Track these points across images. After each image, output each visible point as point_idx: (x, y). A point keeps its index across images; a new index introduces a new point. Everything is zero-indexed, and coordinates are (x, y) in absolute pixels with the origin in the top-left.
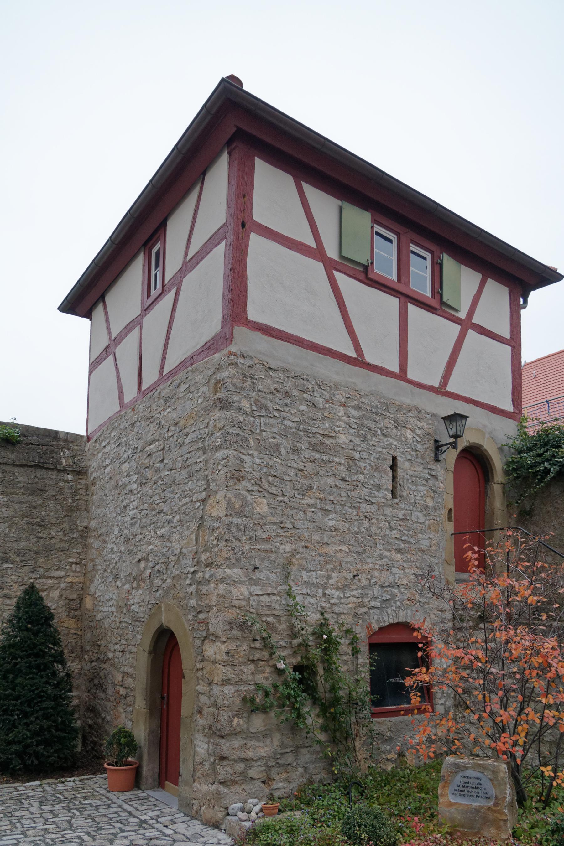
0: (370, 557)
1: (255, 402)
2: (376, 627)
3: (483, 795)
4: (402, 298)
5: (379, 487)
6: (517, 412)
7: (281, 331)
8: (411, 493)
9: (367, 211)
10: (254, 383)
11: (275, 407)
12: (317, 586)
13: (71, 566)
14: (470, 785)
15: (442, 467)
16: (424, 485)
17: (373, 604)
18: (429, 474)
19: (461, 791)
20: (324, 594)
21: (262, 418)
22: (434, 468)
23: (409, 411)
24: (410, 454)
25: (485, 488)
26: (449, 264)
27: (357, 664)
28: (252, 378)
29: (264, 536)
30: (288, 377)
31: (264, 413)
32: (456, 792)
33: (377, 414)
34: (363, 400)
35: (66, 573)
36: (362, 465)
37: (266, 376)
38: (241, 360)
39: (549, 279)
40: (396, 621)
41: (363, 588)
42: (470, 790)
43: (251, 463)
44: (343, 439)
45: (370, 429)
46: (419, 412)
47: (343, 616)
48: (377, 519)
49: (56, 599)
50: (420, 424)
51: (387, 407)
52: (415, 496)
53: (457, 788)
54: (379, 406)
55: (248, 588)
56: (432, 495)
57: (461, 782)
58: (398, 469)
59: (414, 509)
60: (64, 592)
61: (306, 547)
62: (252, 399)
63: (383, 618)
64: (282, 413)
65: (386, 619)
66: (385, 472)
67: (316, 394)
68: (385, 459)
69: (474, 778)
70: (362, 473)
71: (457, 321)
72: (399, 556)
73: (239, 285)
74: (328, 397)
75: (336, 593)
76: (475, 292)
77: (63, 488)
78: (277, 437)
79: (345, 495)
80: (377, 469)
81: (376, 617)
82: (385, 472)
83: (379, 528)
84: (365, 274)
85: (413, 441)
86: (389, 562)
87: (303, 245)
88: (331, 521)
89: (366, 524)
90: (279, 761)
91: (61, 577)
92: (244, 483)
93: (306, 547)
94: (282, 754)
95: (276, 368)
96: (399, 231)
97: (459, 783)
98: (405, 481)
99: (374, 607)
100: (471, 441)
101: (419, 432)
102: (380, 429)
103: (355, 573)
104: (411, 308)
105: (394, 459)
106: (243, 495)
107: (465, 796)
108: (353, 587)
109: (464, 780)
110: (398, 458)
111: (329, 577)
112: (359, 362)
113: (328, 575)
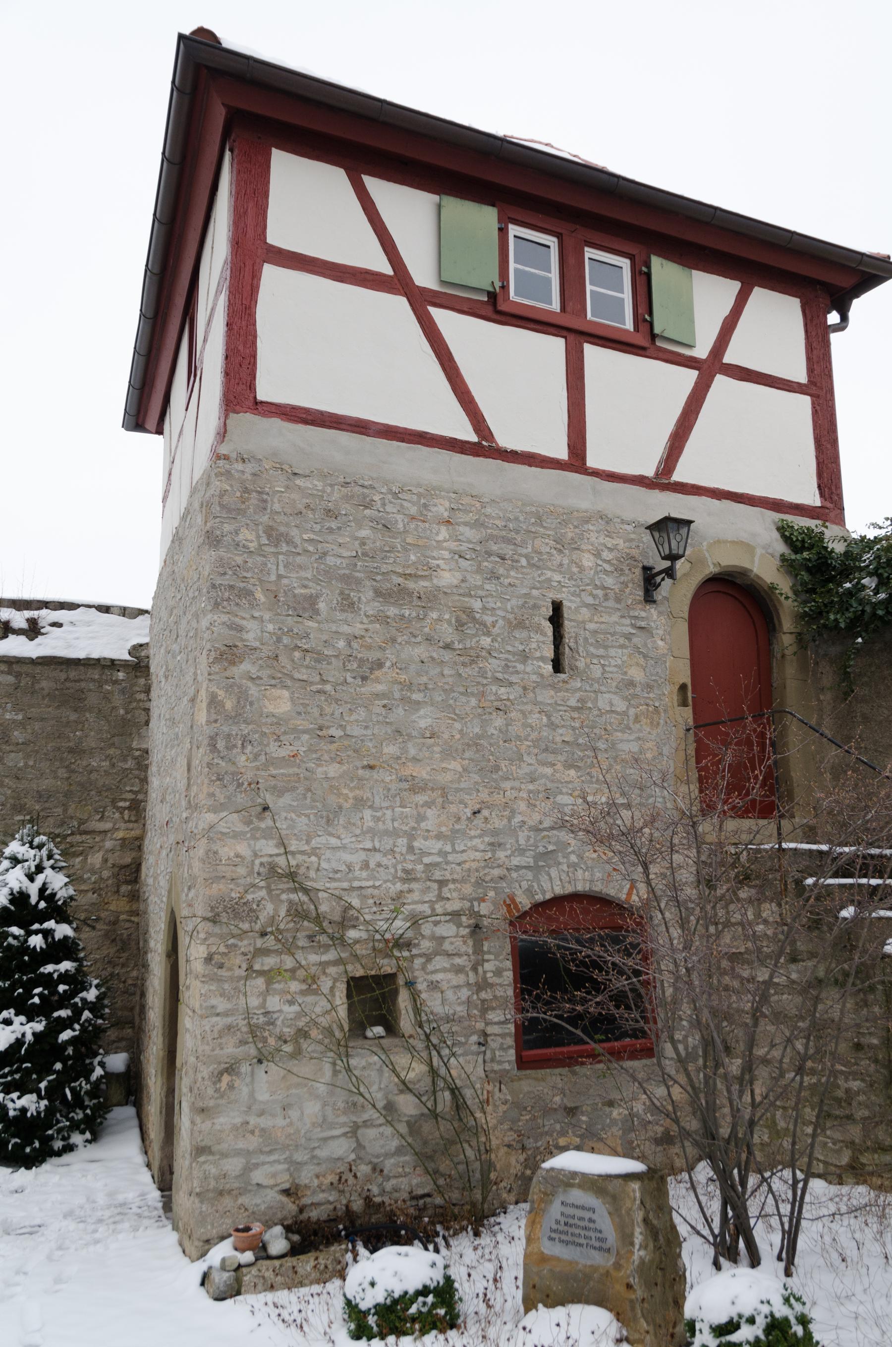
0: (508, 779)
1: (264, 532)
2: (525, 903)
3: (597, 1244)
4: (571, 337)
5: (524, 657)
6: (828, 505)
7: (321, 413)
8: (595, 661)
9: (493, 205)
10: (265, 501)
11: (305, 537)
12: (395, 833)
13: (122, 813)
14: (576, 1221)
15: (660, 613)
16: (622, 647)
17: (516, 861)
18: (633, 626)
19: (561, 1233)
20: (411, 849)
21: (281, 557)
22: (643, 614)
23: (587, 522)
24: (591, 594)
25: (770, 643)
26: (663, 271)
27: (485, 972)
28: (259, 492)
29: (283, 753)
30: (332, 486)
31: (284, 548)
32: (553, 1235)
33: (517, 532)
34: (488, 510)
35: (115, 824)
36: (489, 619)
37: (287, 487)
38: (240, 466)
39: (875, 276)
40: (569, 889)
41: (495, 833)
42: (577, 1231)
43: (258, 631)
44: (447, 578)
45: (503, 559)
46: (609, 521)
47: (451, 886)
48: (523, 712)
49: (98, 866)
50: (610, 542)
51: (540, 518)
52: (603, 666)
53: (555, 1227)
54: (521, 518)
55: (249, 845)
56: (642, 661)
57: (562, 1214)
58: (566, 623)
59: (603, 689)
60: (110, 855)
61: (371, 767)
62: (260, 527)
63: (540, 885)
64: (320, 546)
65: (546, 885)
66: (539, 630)
67: (389, 508)
68: (535, 607)
69: (583, 1208)
70: (488, 634)
71: (690, 363)
72: (572, 772)
73: (241, 348)
74: (413, 510)
75: (436, 846)
76: (727, 312)
77: (109, 692)
78: (311, 584)
79: (453, 672)
80: (521, 625)
81: (525, 885)
82: (539, 630)
83: (525, 725)
84: (495, 308)
85: (597, 573)
86: (549, 785)
87: (367, 272)
88: (424, 719)
89: (499, 721)
90: (318, 1152)
91: (105, 832)
92: (246, 666)
93: (371, 767)
94: (325, 1139)
95: (307, 472)
96: (559, 231)
97: (559, 1217)
98: (581, 641)
99: (518, 868)
100: (723, 564)
101: (606, 555)
102: (526, 556)
103: (476, 808)
104: (590, 350)
105: (557, 607)
106: (240, 687)
107: (567, 1243)
108: (473, 833)
109: (570, 1211)
110: (565, 603)
111: (421, 818)
112: (484, 447)
113: (419, 814)
